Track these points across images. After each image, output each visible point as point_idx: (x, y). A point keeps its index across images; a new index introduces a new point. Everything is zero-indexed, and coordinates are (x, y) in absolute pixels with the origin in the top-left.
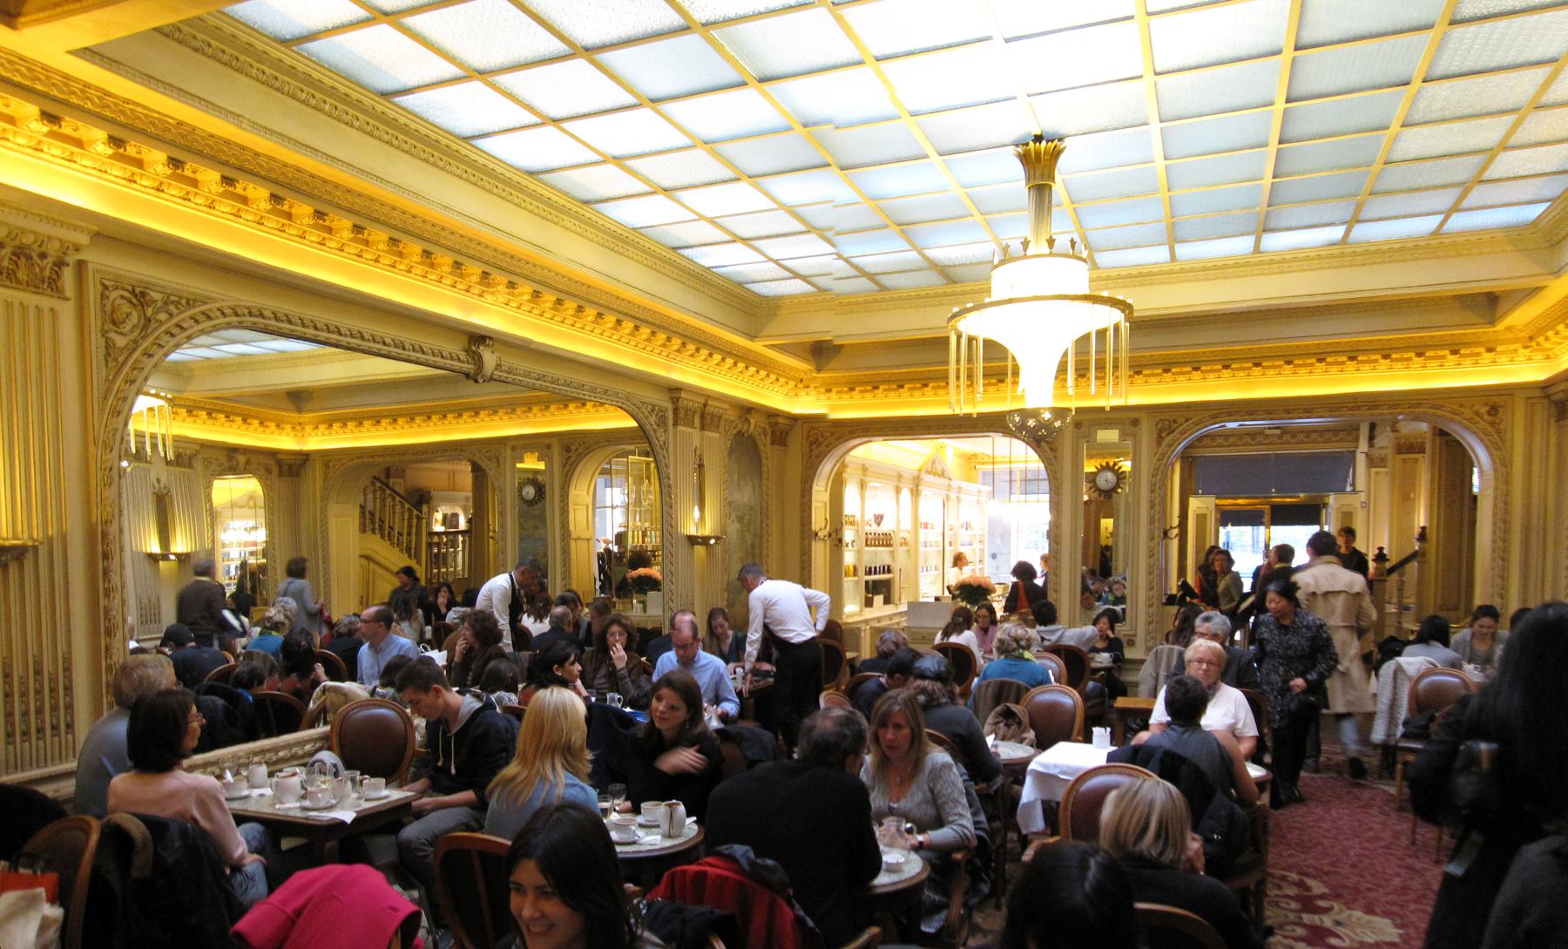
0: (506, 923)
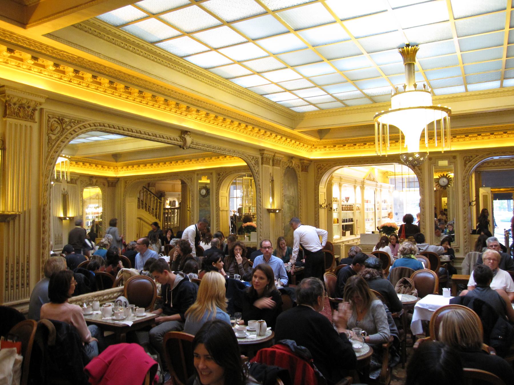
0: (192, 371)
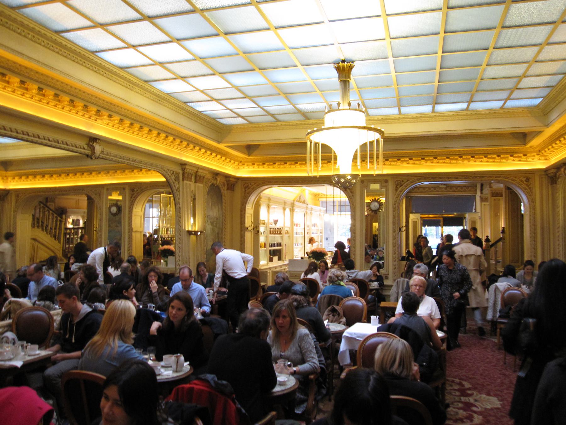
0: (96, 412)
